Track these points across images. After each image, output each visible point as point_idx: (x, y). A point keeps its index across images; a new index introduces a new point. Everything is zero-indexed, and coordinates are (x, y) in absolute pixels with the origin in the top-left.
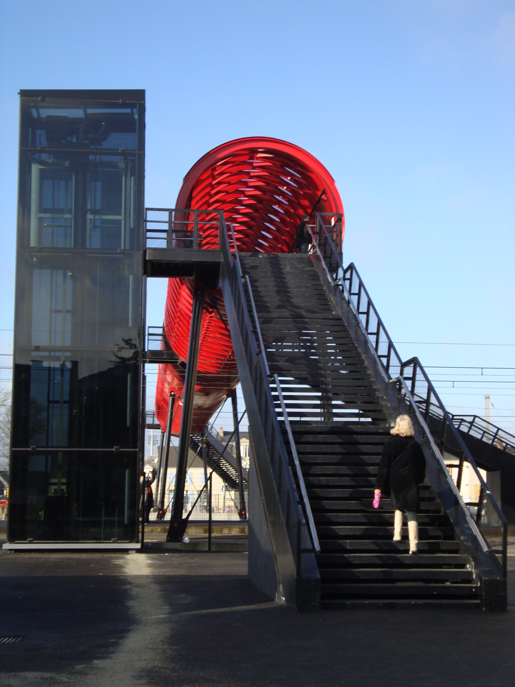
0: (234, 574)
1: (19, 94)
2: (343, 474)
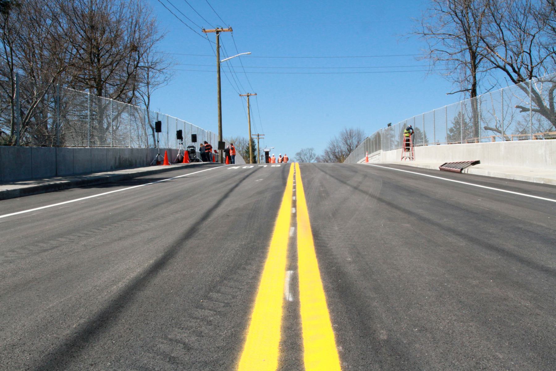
0: (433, 168)
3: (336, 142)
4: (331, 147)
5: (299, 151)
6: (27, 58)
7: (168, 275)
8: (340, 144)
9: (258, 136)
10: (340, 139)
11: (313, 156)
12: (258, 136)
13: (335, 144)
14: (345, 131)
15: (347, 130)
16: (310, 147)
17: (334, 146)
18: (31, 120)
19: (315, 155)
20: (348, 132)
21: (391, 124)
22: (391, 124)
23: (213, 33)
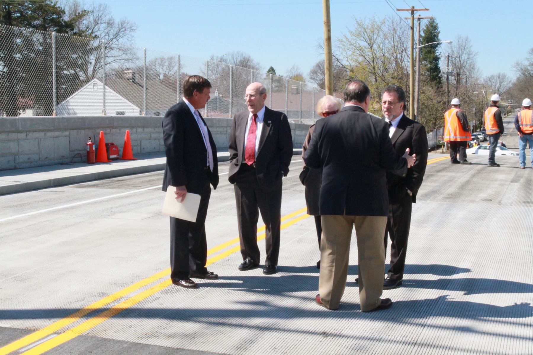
1: (516, 304)
2: (207, 287)
9: (413, 13)
12: (413, 13)
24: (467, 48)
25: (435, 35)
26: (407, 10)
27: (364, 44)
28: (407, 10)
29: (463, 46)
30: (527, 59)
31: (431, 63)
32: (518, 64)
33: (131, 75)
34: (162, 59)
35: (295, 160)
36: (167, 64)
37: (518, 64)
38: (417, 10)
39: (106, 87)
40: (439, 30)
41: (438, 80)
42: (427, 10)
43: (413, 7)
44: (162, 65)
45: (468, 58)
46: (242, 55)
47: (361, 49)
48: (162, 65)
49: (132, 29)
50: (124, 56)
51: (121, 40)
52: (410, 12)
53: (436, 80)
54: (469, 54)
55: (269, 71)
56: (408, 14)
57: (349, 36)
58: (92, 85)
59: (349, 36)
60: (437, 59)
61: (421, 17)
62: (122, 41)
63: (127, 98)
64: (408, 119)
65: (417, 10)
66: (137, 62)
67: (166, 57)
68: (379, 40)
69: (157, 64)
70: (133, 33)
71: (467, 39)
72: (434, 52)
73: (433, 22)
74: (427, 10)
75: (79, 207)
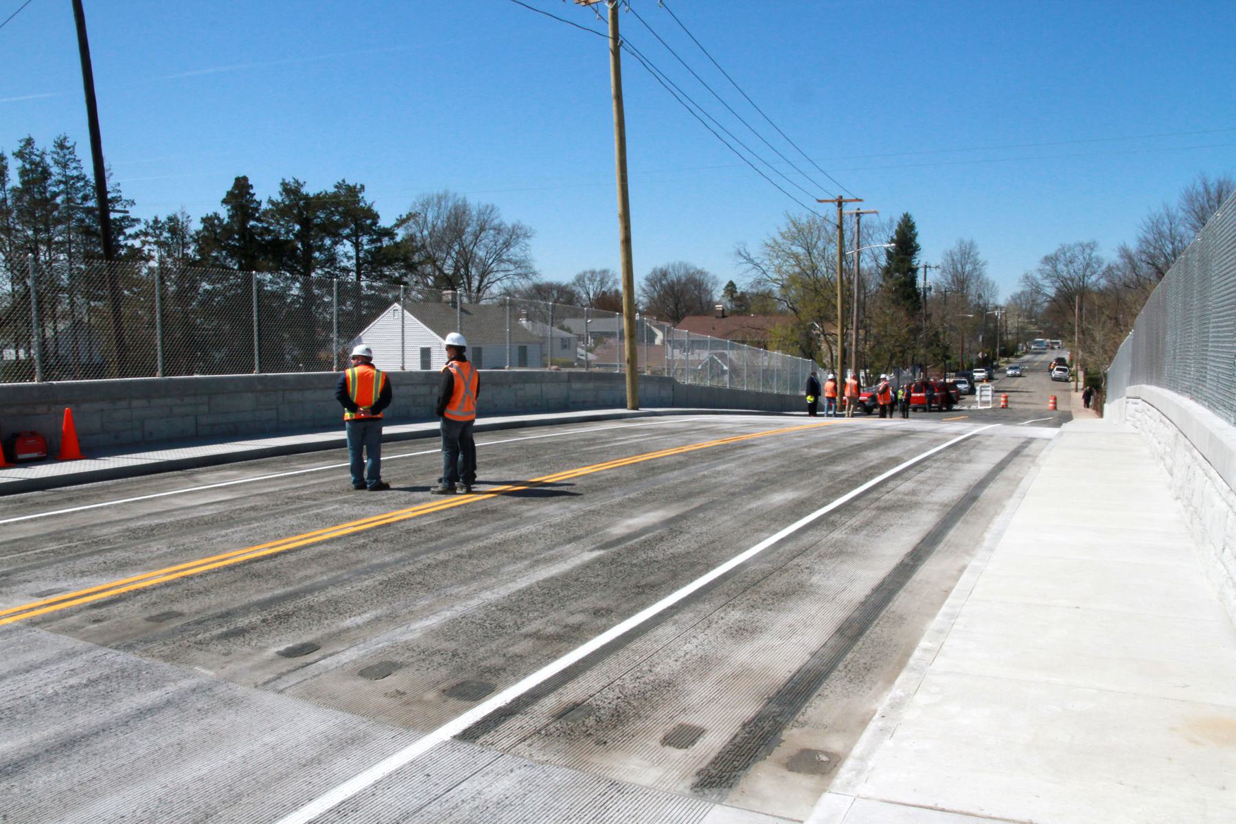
1: (224, 202)
3: (1166, 221)
4: (1150, 237)
5: (1051, 250)
6: (389, 263)
7: (176, 790)
8: (1182, 229)
9: (840, 204)
10: (1181, 214)
11: (1096, 266)
12: (840, 204)
13: (1165, 229)
14: (1201, 189)
15: (1209, 183)
16: (1086, 241)
17: (1160, 234)
18: (635, 476)
19: (1099, 263)
20: (1212, 190)
21: (156, 218)
22: (156, 218)
23: (394, 222)
24: (973, 256)
25: (910, 238)
26: (833, 201)
27: (800, 250)
28: (833, 201)
29: (966, 253)
30: (1040, 270)
31: (905, 274)
32: (1027, 277)
33: (450, 297)
34: (593, 273)
35: (390, 453)
36: (598, 279)
37: (1027, 277)
38: (846, 201)
39: (405, 311)
40: (916, 230)
41: (915, 298)
42: (861, 200)
43: (841, 197)
44: (592, 280)
45: (975, 269)
46: (685, 266)
47: (796, 256)
48: (592, 280)
49: (526, 236)
50: (519, 271)
51: (512, 250)
52: (837, 203)
53: (912, 298)
54: (975, 263)
55: (728, 286)
56: (832, 209)
57: (779, 239)
58: (392, 311)
59: (779, 239)
60: (914, 271)
61: (861, 211)
62: (515, 252)
63: (432, 329)
64: (664, 377)
65: (846, 201)
66: (534, 278)
67: (598, 269)
68: (820, 244)
69: (586, 279)
70: (527, 241)
71: (972, 244)
72: (910, 261)
73: (909, 220)
74: (861, 200)
75: (102, 508)
